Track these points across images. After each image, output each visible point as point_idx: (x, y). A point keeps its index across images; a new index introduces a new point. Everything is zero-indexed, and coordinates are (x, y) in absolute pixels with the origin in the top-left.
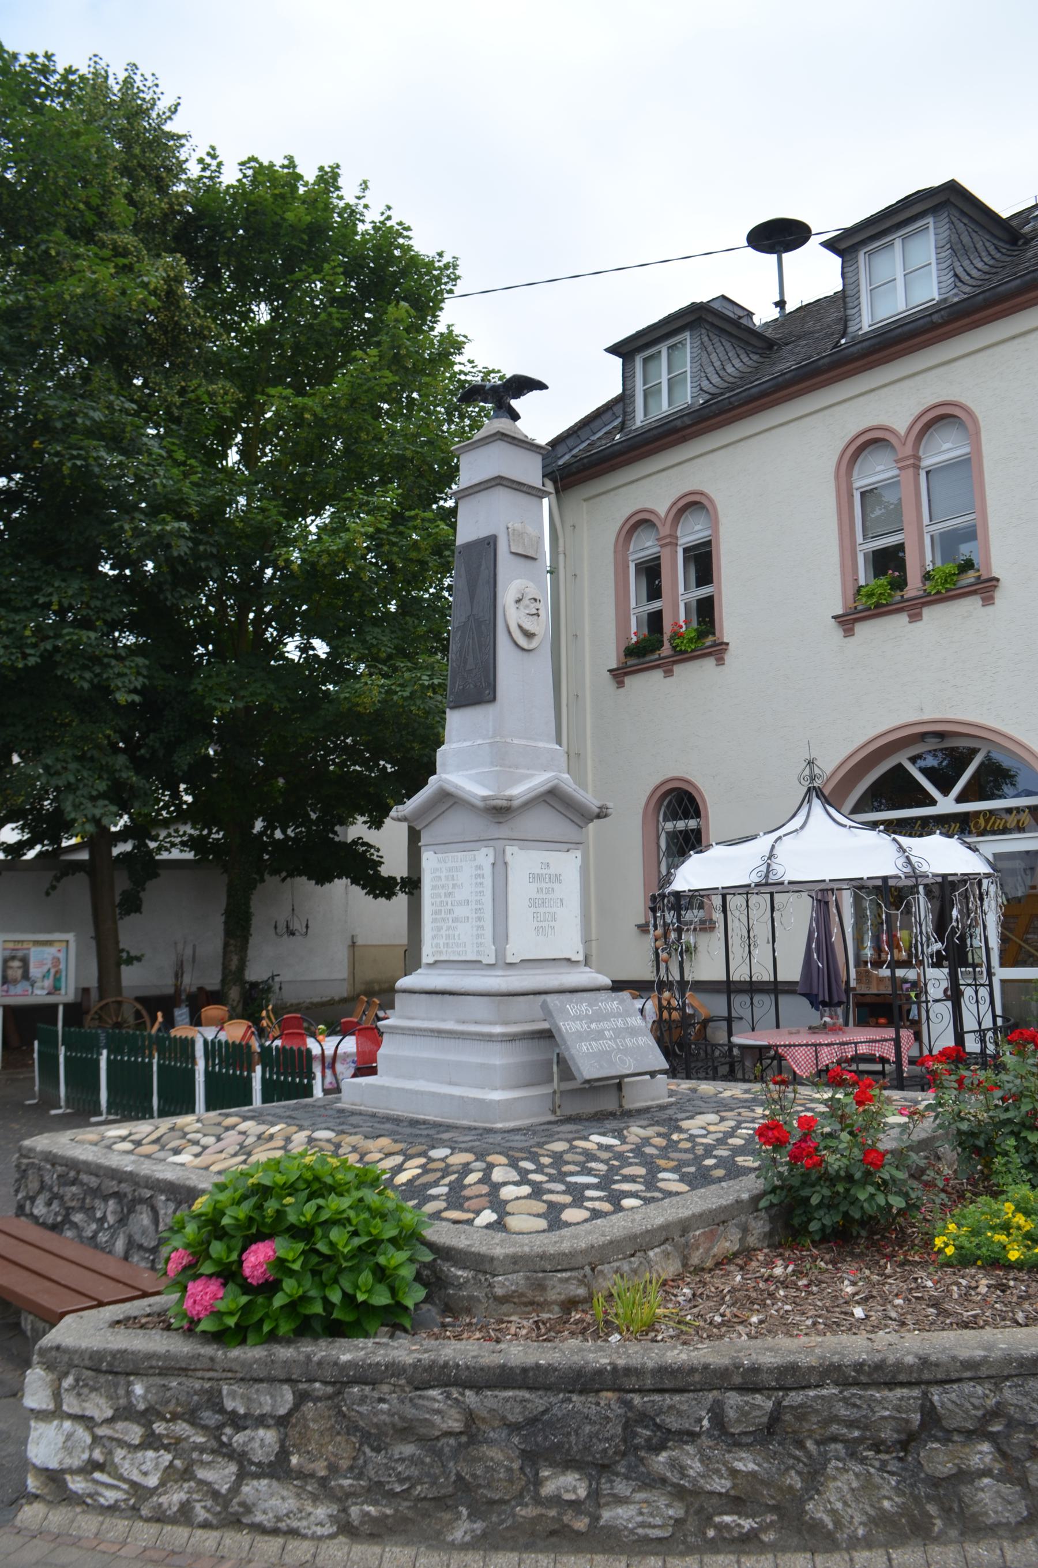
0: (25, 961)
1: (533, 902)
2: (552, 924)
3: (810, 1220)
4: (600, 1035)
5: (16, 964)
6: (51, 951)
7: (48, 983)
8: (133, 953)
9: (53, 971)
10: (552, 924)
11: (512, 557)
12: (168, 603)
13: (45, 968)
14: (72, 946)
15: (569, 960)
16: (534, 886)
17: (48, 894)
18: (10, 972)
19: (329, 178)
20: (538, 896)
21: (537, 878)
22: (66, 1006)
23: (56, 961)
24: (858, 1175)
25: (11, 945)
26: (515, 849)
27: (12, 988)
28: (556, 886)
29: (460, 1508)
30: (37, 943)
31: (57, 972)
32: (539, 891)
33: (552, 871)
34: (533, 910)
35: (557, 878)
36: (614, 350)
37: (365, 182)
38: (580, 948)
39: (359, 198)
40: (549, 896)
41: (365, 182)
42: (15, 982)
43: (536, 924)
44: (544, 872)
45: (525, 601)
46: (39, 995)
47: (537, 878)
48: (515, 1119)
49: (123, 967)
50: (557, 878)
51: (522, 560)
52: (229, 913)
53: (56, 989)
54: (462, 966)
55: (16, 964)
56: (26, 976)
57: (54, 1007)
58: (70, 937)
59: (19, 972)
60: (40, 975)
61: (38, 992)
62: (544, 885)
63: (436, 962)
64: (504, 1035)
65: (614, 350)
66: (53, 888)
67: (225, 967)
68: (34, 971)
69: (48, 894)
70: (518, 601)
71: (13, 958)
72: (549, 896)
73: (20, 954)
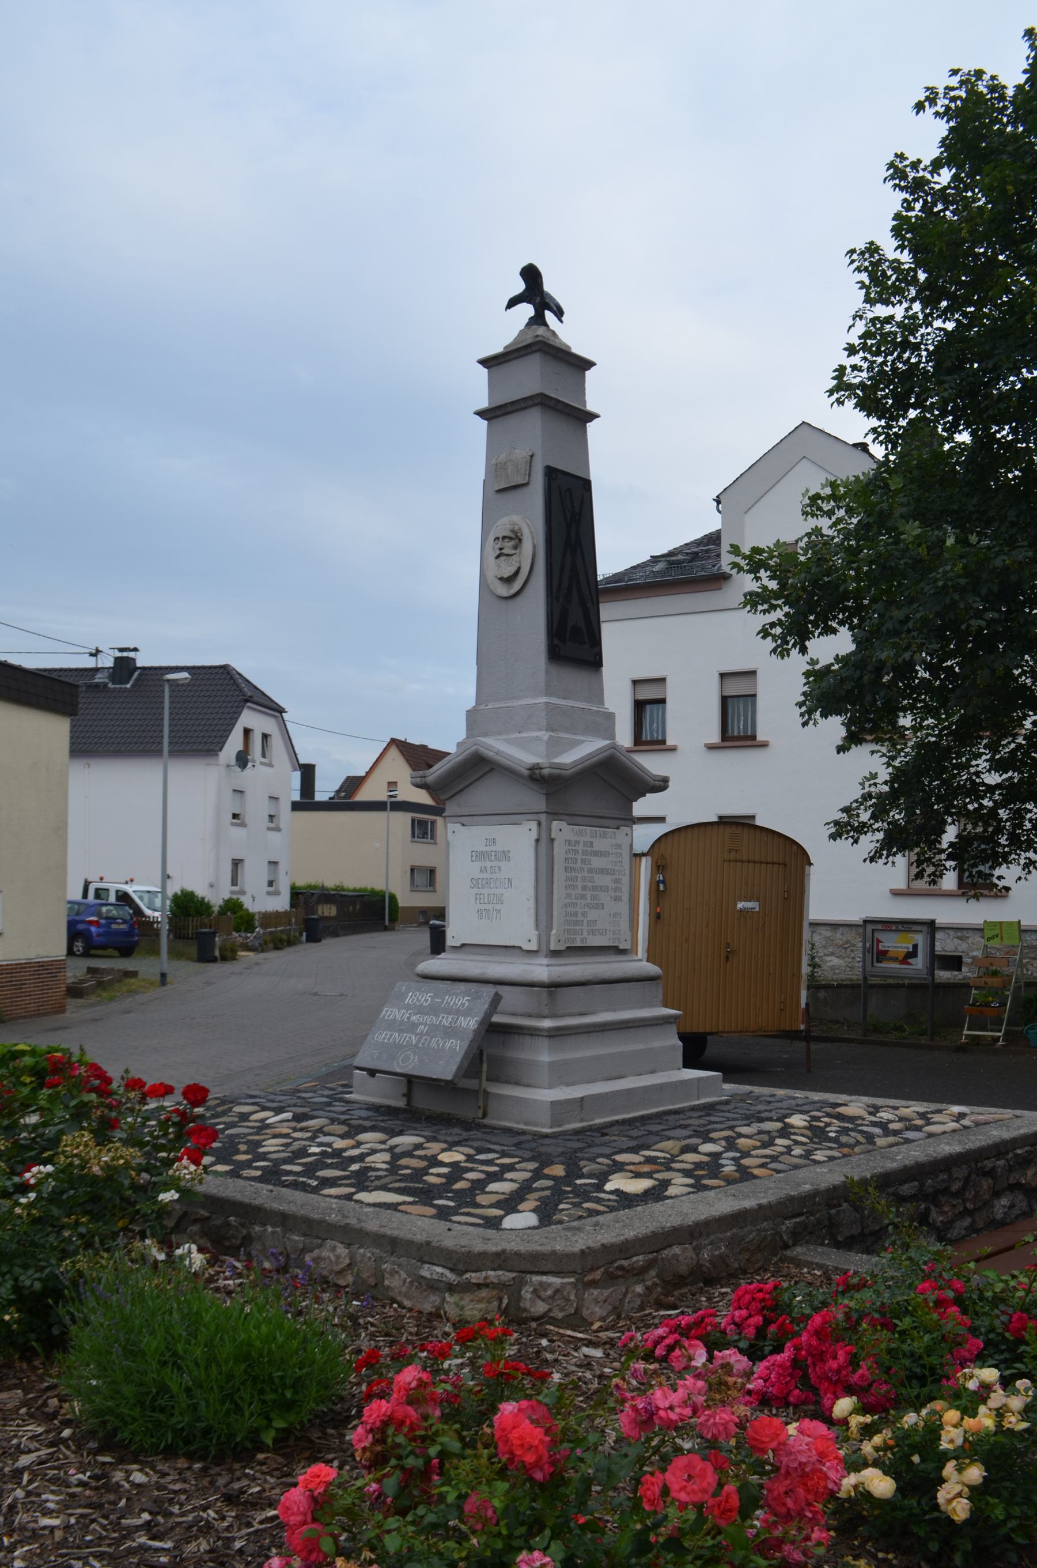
1: (475, 883)
2: (498, 907)
3: (50, 1326)
10: (498, 907)
15: (520, 948)
16: (477, 865)
20: (481, 876)
21: (480, 856)
24: (133, 1254)
28: (503, 864)
29: (960, 1510)
32: (483, 870)
33: (498, 848)
34: (475, 891)
35: (506, 855)
36: (485, 362)
38: (533, 934)
40: (494, 876)
47: (480, 856)
50: (506, 855)
54: (502, 950)
62: (488, 864)
63: (463, 945)
64: (550, 1029)
65: (485, 362)
72: (494, 876)
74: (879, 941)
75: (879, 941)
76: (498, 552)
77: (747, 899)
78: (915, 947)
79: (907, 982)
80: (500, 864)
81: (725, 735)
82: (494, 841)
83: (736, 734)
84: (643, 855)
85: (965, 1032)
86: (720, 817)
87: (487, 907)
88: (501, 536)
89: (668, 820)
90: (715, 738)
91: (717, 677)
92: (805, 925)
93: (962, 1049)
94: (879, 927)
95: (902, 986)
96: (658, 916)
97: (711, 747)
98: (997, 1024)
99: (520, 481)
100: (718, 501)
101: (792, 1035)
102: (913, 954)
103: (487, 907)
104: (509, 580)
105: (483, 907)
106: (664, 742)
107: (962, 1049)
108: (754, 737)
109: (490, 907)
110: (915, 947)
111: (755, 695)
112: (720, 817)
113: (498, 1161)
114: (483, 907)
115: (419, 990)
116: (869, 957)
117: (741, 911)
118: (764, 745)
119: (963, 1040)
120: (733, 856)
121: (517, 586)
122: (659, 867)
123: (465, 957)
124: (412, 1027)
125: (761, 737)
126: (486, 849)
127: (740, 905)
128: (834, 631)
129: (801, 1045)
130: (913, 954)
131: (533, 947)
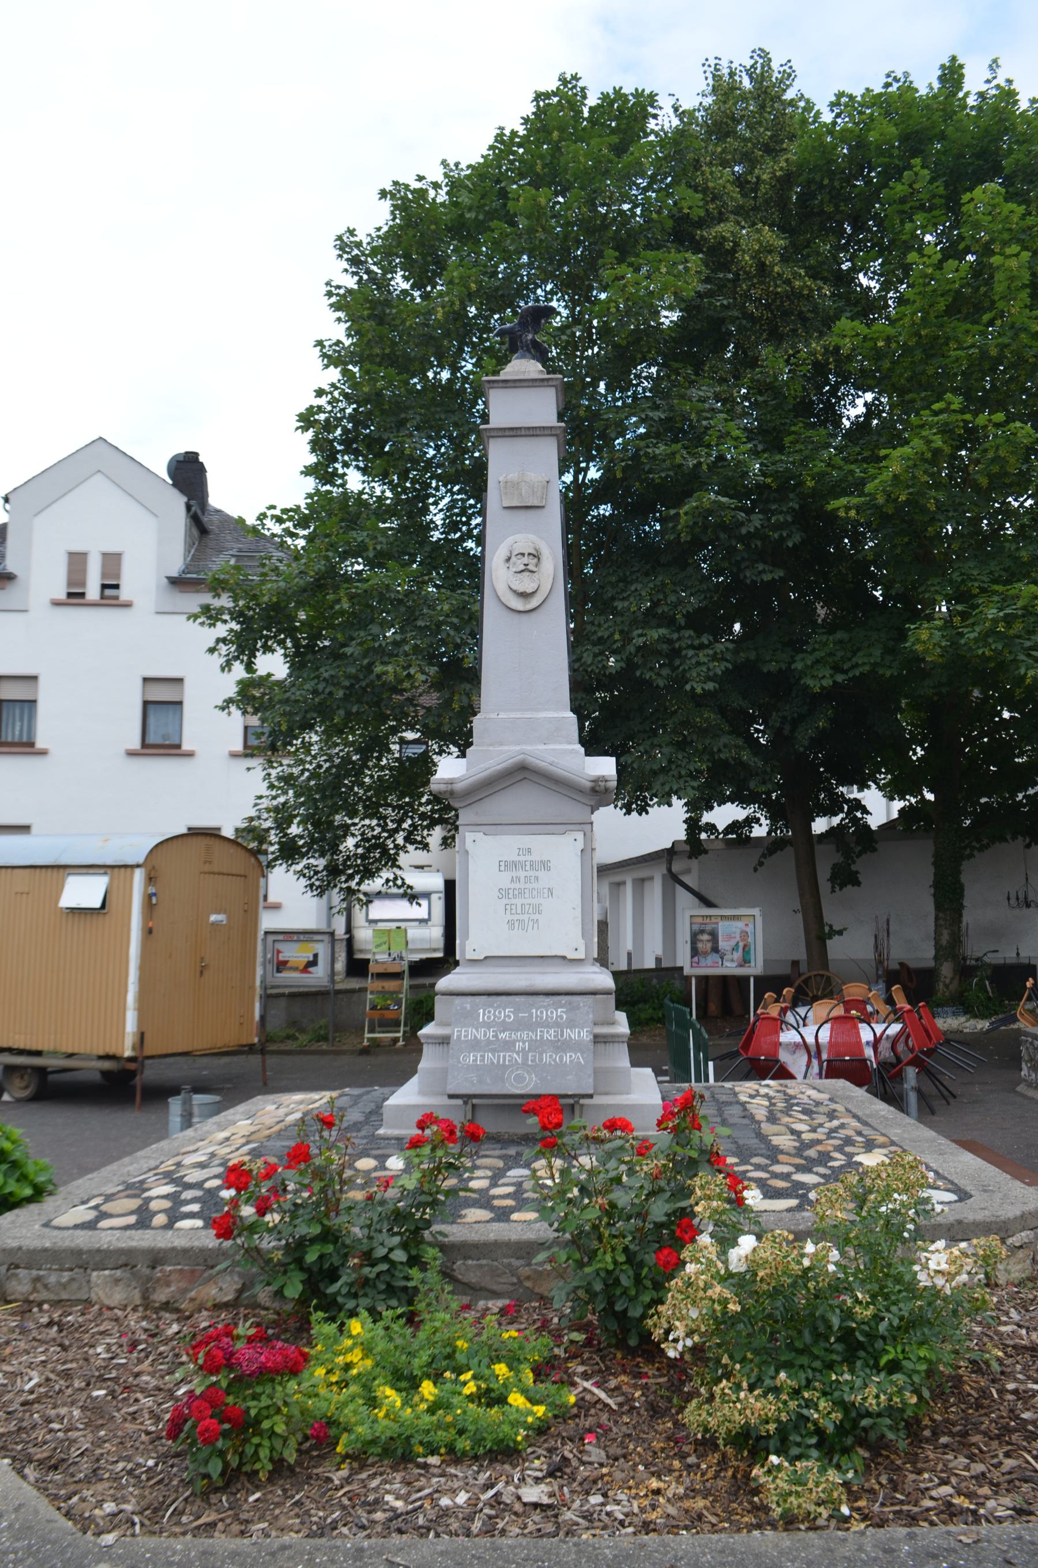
0: (714, 935)
2: (536, 917)
4: (508, 1045)
5: (705, 937)
6: (739, 925)
7: (737, 955)
8: (836, 928)
9: (741, 944)
11: (507, 512)
12: (748, 581)
13: (733, 943)
14: (759, 920)
15: (564, 958)
16: (507, 876)
17: (755, 870)
18: (700, 945)
19: (952, 74)
20: (513, 886)
22: (756, 978)
23: (744, 934)
25: (700, 920)
26: (479, 836)
27: (702, 960)
28: (541, 874)
30: (723, 917)
31: (745, 946)
33: (535, 857)
34: (505, 901)
35: (545, 865)
37: (995, 61)
39: (988, 81)
40: (530, 886)
41: (995, 61)
42: (705, 954)
43: (509, 917)
44: (522, 858)
45: (513, 559)
46: (730, 967)
48: (400, 1128)
49: (828, 942)
51: (522, 515)
52: (937, 885)
53: (745, 961)
54: (528, 961)
55: (705, 937)
56: (715, 949)
57: (745, 979)
58: (756, 911)
59: (709, 945)
60: (729, 948)
61: (728, 964)
62: (522, 874)
63: (486, 958)
66: (761, 864)
67: (937, 941)
68: (722, 944)
69: (755, 870)
70: (508, 560)
71: (702, 932)
73: (709, 928)
74: (279, 952)
75: (279, 952)
76: (522, 567)
77: (218, 912)
78: (316, 956)
79: (287, 991)
80: (537, 874)
81: (144, 745)
82: (529, 851)
83: (10, 739)
84: (138, 866)
85: (367, 1035)
86: (189, 829)
87: (521, 917)
88: (526, 552)
89: (34, 830)
90: (135, 744)
91: (140, 682)
92: (261, 934)
93: (365, 1052)
94: (281, 937)
95: (283, 995)
96: (150, 931)
97: (131, 754)
98: (395, 1024)
99: (536, 503)
100: (6, 500)
101: (251, 1049)
102: (314, 963)
103: (521, 917)
104: (524, 595)
105: (516, 917)
106: (179, 746)
107: (365, 1052)
108: (31, 744)
109: (525, 917)
110: (316, 956)
111: (35, 701)
112: (189, 829)
113: (750, 1168)
114: (516, 917)
115: (491, 1006)
116: (269, 967)
117: (213, 924)
118: (43, 753)
119: (366, 1043)
120: (207, 868)
121: (534, 602)
122: (150, 879)
123: (491, 970)
124: (508, 1045)
125: (40, 744)
126: (517, 859)
127: (213, 918)
128: (273, 651)
129: (255, 1060)
130: (314, 963)
131: (581, 955)
